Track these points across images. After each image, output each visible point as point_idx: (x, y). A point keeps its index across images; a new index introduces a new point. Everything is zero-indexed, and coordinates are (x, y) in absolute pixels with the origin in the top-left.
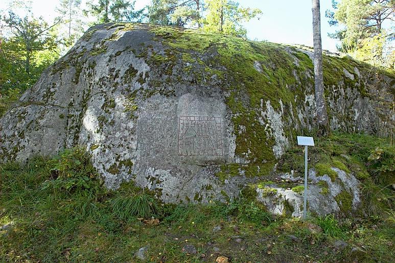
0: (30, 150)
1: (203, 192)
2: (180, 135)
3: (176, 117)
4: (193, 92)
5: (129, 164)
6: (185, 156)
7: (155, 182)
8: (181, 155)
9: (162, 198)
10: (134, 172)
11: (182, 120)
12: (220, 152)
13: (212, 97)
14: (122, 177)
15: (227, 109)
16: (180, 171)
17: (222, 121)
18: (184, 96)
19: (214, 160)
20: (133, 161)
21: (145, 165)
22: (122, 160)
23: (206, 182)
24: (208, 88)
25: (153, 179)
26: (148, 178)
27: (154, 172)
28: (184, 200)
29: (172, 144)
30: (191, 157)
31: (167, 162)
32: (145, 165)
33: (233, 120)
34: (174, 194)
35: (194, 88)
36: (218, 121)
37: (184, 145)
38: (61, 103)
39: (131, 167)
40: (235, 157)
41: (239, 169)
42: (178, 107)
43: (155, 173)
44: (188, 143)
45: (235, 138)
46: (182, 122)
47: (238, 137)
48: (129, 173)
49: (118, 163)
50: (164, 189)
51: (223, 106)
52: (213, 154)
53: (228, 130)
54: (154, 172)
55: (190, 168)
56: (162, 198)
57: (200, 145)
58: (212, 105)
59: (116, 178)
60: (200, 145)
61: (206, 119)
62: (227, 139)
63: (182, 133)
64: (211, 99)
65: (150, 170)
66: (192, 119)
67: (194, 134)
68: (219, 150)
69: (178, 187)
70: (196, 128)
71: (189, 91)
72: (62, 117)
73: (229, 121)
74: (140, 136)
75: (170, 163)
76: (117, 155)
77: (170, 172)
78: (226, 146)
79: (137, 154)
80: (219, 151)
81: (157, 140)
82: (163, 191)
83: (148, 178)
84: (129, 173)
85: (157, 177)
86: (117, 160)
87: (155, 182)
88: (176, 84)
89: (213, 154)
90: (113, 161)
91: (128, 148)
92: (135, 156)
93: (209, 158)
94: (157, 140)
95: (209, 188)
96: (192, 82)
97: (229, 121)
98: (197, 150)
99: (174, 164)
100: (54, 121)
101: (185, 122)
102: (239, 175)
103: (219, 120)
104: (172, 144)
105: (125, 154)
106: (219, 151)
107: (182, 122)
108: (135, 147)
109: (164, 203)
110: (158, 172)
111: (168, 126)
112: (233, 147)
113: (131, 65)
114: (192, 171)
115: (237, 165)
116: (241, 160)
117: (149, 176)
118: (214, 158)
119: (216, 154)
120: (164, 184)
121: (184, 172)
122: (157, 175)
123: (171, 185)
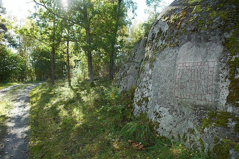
0: (123, 87)
1: (188, 135)
2: (177, 80)
3: (175, 65)
4: (193, 40)
5: (147, 101)
6: (180, 98)
7: (157, 116)
8: (177, 97)
9: (158, 130)
10: (149, 107)
11: (180, 67)
12: (210, 98)
13: (210, 41)
14: (141, 109)
15: (224, 51)
16: (176, 111)
17: (216, 64)
18: (184, 45)
19: (202, 104)
20: (149, 99)
21: (155, 103)
22: (144, 97)
23: (191, 125)
24: (208, 33)
25: (157, 114)
26: (154, 113)
27: (159, 108)
28: (176, 136)
29: (171, 87)
30: (184, 100)
31: (167, 101)
32: (155, 103)
33: (229, 63)
34: (168, 129)
35: (193, 36)
36: (211, 65)
37: (179, 89)
38: (138, 60)
39: (147, 103)
40: (226, 104)
41: (230, 120)
42: (178, 55)
43: (160, 110)
44: (182, 87)
45: (228, 82)
46: (179, 68)
47: (232, 82)
48: (146, 107)
49: (142, 99)
50: (161, 123)
51: (219, 49)
52: (203, 99)
53: (221, 75)
54: (159, 108)
55: (184, 109)
56: (158, 130)
57: (191, 89)
58: (208, 49)
59: (139, 109)
60: (191, 89)
61: (199, 64)
62: (218, 85)
63: (178, 78)
64: (208, 44)
65: (157, 106)
66: (187, 65)
67: (187, 79)
68: (208, 95)
69: (171, 124)
70: (189, 74)
71: (189, 40)
72: (136, 68)
73: (224, 65)
74: (154, 81)
75: (169, 103)
76: (142, 93)
77: (169, 111)
78: (217, 92)
79: (151, 93)
80: (208, 97)
81: (162, 84)
82: (160, 125)
83: (154, 113)
84: (146, 107)
85: (160, 113)
86: (142, 97)
87: (157, 116)
88: (181, 36)
89: (203, 99)
90: (140, 97)
91: (148, 89)
92: (150, 95)
93: (198, 103)
94: (162, 84)
95: (192, 131)
96: (194, 31)
97: (224, 65)
98: (188, 94)
99: (172, 104)
100: (133, 71)
101: (182, 68)
102: (226, 126)
103: (213, 63)
104: (171, 87)
105: (146, 93)
106: (208, 97)
107: (179, 68)
108: (151, 89)
109: (159, 135)
110: (161, 109)
111: (169, 72)
112: (225, 93)
113: (161, 28)
114: (185, 112)
115: (229, 114)
116: (233, 110)
117: (155, 111)
118: (202, 103)
119: (205, 99)
120: (162, 119)
121: (179, 112)
122: (160, 111)
123: (167, 122)
